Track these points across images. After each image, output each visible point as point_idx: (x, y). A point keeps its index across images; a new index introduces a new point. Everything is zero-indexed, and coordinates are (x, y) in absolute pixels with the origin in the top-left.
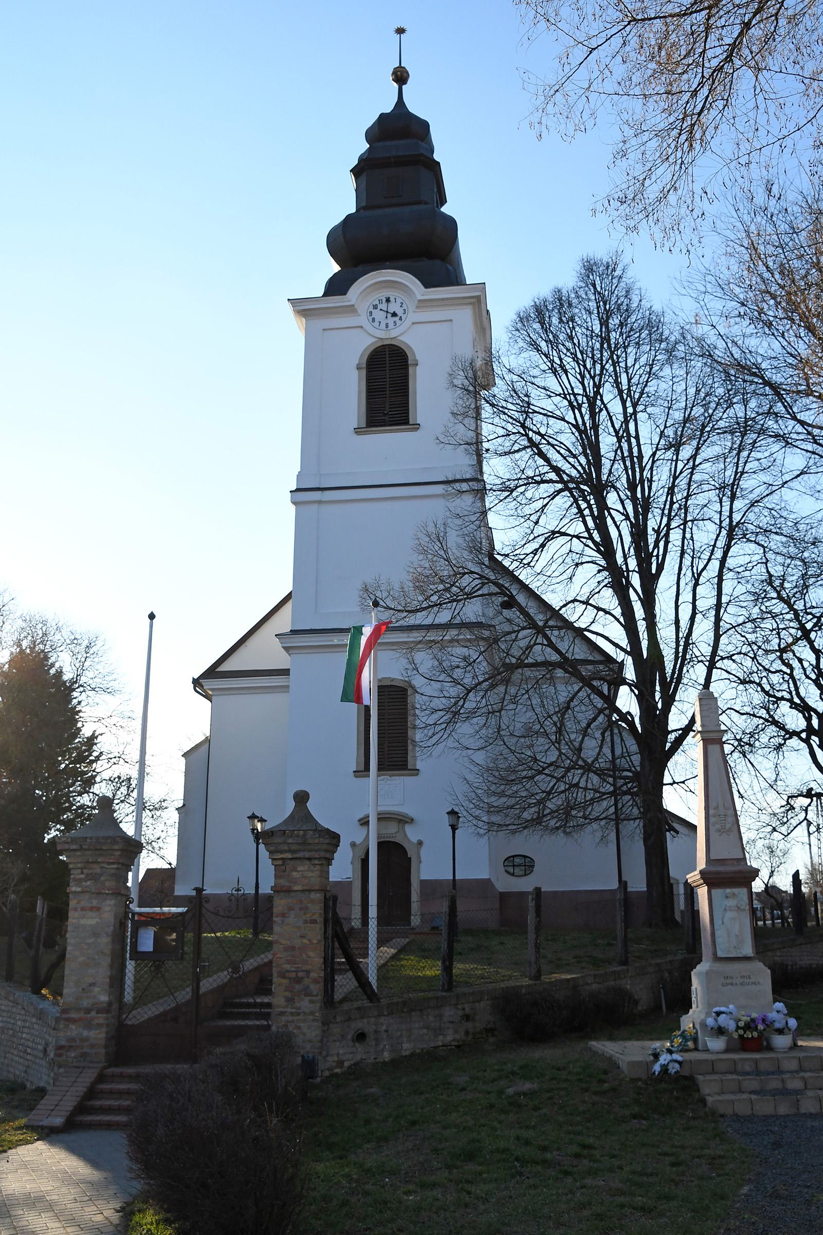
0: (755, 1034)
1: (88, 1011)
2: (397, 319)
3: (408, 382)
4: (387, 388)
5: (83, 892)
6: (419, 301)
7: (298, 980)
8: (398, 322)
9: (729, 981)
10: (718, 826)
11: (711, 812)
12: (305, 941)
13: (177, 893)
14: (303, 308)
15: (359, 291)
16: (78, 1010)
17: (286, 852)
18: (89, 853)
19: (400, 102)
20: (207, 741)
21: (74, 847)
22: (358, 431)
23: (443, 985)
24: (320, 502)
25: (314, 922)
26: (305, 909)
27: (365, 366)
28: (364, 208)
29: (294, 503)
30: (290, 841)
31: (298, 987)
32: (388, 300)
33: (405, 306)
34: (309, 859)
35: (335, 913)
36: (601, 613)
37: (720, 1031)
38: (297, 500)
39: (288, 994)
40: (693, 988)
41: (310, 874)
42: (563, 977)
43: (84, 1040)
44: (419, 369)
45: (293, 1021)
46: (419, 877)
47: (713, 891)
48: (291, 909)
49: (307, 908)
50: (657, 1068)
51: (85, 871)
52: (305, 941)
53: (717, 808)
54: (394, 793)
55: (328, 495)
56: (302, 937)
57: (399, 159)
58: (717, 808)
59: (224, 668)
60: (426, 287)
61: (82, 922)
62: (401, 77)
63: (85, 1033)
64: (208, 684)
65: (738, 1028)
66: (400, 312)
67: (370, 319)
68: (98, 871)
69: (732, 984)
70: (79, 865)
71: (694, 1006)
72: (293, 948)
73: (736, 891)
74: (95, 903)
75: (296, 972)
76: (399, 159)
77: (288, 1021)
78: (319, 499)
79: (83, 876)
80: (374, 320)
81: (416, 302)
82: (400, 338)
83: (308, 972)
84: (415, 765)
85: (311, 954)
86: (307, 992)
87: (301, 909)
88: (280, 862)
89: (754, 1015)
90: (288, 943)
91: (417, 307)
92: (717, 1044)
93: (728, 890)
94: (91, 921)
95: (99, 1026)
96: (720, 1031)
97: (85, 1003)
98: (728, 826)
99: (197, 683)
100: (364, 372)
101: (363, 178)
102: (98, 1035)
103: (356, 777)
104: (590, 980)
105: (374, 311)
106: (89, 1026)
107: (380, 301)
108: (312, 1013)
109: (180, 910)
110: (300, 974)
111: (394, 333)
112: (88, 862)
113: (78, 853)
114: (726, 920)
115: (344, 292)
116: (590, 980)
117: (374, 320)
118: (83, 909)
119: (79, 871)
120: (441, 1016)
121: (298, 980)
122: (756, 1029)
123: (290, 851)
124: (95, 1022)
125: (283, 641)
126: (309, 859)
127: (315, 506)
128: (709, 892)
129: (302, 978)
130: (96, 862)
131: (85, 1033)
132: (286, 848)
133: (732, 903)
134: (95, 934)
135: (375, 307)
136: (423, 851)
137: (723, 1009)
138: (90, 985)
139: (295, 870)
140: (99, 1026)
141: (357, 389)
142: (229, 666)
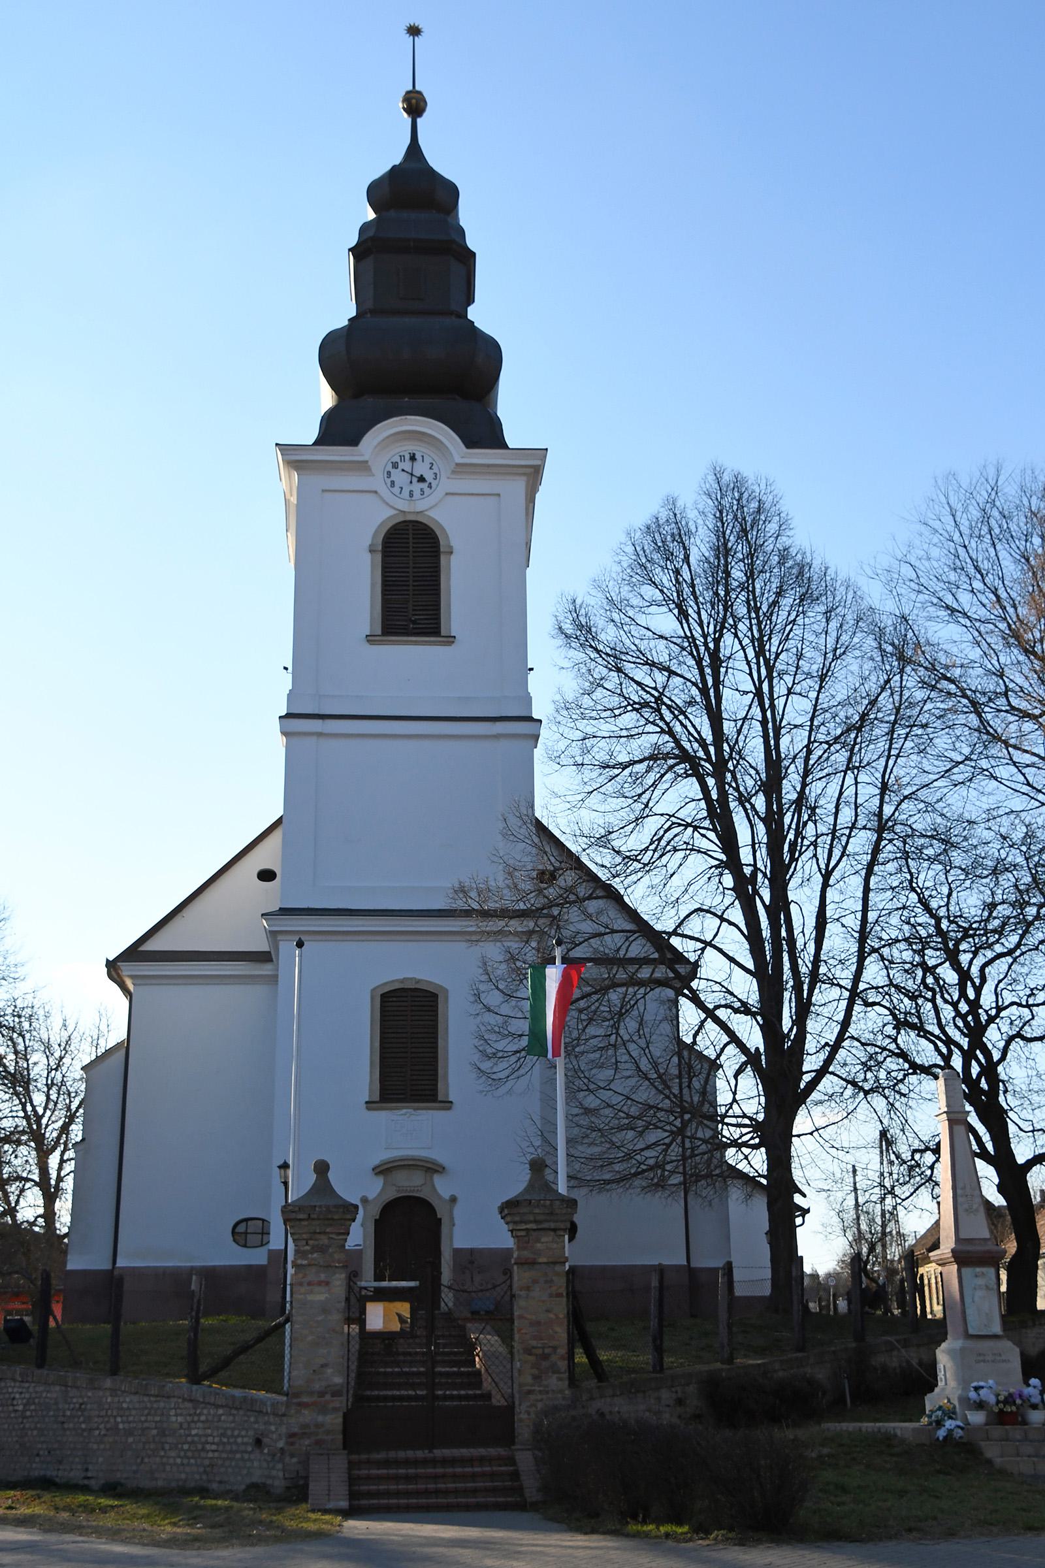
0: (1014, 1408)
1: (322, 1394)
2: (424, 486)
3: (439, 576)
4: (411, 583)
5: (309, 1265)
6: (457, 464)
7: (545, 1357)
8: (427, 491)
9: (981, 1358)
10: (966, 1206)
11: (959, 1192)
12: (552, 1316)
13: (69, 1267)
14: (292, 456)
15: (375, 442)
16: (311, 1393)
17: (531, 1222)
18: (317, 1222)
19: (414, 149)
20: (125, 1047)
21: (301, 1216)
22: (371, 639)
23: (654, 1366)
24: (320, 735)
25: (559, 1295)
26: (550, 1282)
27: (380, 548)
28: (373, 312)
29: (284, 733)
30: (537, 1211)
31: (545, 1364)
32: (413, 458)
33: (435, 469)
34: (554, 1230)
35: (573, 1287)
36: (725, 924)
37: (980, 1405)
38: (289, 730)
39: (536, 1372)
40: (940, 1366)
41: (555, 1246)
42: (751, 1362)
43: (318, 1426)
44: (453, 558)
45: (541, 1400)
46: (452, 1244)
47: (964, 1270)
48: (535, 1282)
49: (552, 1281)
50: (941, 1433)
51: (311, 1242)
52: (552, 1316)
53: (964, 1188)
54: (409, 1131)
55: (500, 728)
56: (548, 1311)
57: (413, 237)
58: (964, 1188)
59: (142, 948)
60: (468, 447)
61: (310, 1297)
62: (415, 105)
63: (320, 1419)
64: (126, 969)
65: (998, 1402)
66: (429, 476)
67: (388, 481)
68: (326, 1241)
69: (984, 1361)
70: (305, 1236)
71: (941, 1384)
72: (538, 1323)
73: (984, 1270)
74: (323, 1277)
75: (543, 1348)
76: (413, 237)
77: (537, 1401)
78: (320, 730)
79: (308, 1248)
80: (393, 483)
81: (453, 465)
82: (431, 513)
83: (555, 1348)
84: (447, 1095)
85: (558, 1329)
86: (554, 1369)
87: (546, 1282)
88: (523, 1233)
89: (1012, 1390)
90: (534, 1317)
91: (453, 472)
92: (977, 1418)
93: (978, 1270)
94: (319, 1296)
95: (335, 1409)
96: (980, 1405)
97: (317, 1386)
98: (975, 1207)
99: (113, 968)
100: (379, 557)
101: (369, 262)
102: (334, 1421)
103: (368, 1109)
104: (777, 1366)
105: (393, 471)
106: (323, 1410)
107: (402, 458)
108: (561, 1391)
109: (412, 1284)
110: (547, 1351)
111: (420, 506)
112: (315, 1233)
113: (306, 1223)
114: (976, 1299)
115: (354, 441)
116: (777, 1366)
117: (393, 483)
118: (309, 1284)
119: (304, 1242)
120: (659, 1399)
121: (545, 1357)
122: (1014, 1403)
123: (535, 1222)
124: (331, 1406)
125: (271, 922)
126: (554, 1230)
127: (314, 739)
128: (959, 1270)
129: (549, 1355)
130: (325, 1233)
131: (320, 1419)
132: (532, 1218)
133: (980, 1281)
134: (325, 1311)
135: (395, 465)
136: (458, 1211)
137: (982, 1384)
138: (322, 1366)
139: (538, 1241)
140: (335, 1409)
141: (369, 582)
142: (155, 945)
